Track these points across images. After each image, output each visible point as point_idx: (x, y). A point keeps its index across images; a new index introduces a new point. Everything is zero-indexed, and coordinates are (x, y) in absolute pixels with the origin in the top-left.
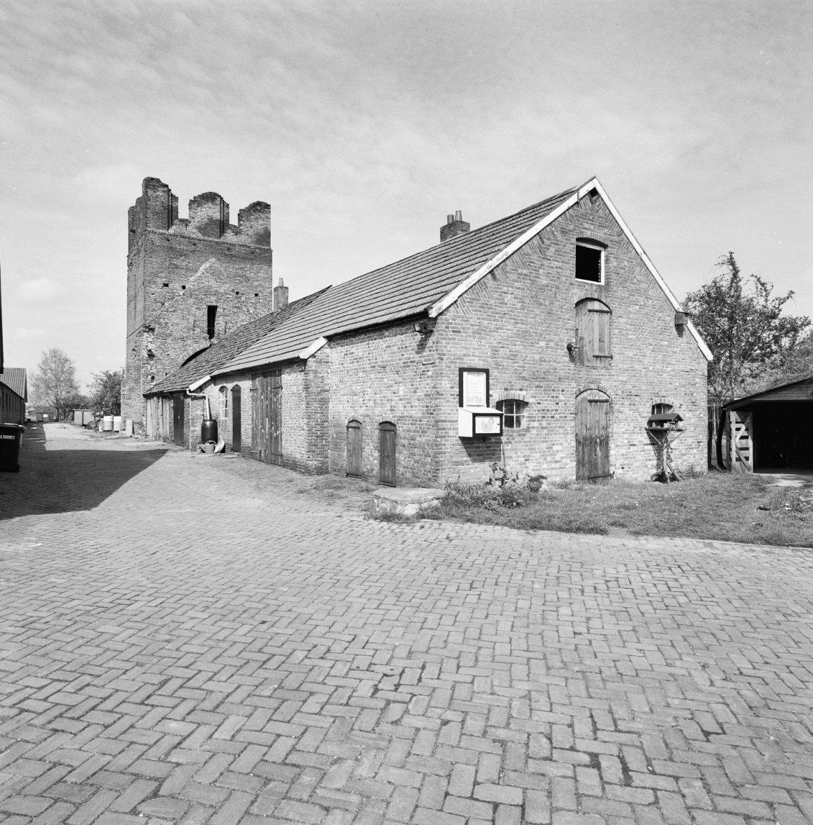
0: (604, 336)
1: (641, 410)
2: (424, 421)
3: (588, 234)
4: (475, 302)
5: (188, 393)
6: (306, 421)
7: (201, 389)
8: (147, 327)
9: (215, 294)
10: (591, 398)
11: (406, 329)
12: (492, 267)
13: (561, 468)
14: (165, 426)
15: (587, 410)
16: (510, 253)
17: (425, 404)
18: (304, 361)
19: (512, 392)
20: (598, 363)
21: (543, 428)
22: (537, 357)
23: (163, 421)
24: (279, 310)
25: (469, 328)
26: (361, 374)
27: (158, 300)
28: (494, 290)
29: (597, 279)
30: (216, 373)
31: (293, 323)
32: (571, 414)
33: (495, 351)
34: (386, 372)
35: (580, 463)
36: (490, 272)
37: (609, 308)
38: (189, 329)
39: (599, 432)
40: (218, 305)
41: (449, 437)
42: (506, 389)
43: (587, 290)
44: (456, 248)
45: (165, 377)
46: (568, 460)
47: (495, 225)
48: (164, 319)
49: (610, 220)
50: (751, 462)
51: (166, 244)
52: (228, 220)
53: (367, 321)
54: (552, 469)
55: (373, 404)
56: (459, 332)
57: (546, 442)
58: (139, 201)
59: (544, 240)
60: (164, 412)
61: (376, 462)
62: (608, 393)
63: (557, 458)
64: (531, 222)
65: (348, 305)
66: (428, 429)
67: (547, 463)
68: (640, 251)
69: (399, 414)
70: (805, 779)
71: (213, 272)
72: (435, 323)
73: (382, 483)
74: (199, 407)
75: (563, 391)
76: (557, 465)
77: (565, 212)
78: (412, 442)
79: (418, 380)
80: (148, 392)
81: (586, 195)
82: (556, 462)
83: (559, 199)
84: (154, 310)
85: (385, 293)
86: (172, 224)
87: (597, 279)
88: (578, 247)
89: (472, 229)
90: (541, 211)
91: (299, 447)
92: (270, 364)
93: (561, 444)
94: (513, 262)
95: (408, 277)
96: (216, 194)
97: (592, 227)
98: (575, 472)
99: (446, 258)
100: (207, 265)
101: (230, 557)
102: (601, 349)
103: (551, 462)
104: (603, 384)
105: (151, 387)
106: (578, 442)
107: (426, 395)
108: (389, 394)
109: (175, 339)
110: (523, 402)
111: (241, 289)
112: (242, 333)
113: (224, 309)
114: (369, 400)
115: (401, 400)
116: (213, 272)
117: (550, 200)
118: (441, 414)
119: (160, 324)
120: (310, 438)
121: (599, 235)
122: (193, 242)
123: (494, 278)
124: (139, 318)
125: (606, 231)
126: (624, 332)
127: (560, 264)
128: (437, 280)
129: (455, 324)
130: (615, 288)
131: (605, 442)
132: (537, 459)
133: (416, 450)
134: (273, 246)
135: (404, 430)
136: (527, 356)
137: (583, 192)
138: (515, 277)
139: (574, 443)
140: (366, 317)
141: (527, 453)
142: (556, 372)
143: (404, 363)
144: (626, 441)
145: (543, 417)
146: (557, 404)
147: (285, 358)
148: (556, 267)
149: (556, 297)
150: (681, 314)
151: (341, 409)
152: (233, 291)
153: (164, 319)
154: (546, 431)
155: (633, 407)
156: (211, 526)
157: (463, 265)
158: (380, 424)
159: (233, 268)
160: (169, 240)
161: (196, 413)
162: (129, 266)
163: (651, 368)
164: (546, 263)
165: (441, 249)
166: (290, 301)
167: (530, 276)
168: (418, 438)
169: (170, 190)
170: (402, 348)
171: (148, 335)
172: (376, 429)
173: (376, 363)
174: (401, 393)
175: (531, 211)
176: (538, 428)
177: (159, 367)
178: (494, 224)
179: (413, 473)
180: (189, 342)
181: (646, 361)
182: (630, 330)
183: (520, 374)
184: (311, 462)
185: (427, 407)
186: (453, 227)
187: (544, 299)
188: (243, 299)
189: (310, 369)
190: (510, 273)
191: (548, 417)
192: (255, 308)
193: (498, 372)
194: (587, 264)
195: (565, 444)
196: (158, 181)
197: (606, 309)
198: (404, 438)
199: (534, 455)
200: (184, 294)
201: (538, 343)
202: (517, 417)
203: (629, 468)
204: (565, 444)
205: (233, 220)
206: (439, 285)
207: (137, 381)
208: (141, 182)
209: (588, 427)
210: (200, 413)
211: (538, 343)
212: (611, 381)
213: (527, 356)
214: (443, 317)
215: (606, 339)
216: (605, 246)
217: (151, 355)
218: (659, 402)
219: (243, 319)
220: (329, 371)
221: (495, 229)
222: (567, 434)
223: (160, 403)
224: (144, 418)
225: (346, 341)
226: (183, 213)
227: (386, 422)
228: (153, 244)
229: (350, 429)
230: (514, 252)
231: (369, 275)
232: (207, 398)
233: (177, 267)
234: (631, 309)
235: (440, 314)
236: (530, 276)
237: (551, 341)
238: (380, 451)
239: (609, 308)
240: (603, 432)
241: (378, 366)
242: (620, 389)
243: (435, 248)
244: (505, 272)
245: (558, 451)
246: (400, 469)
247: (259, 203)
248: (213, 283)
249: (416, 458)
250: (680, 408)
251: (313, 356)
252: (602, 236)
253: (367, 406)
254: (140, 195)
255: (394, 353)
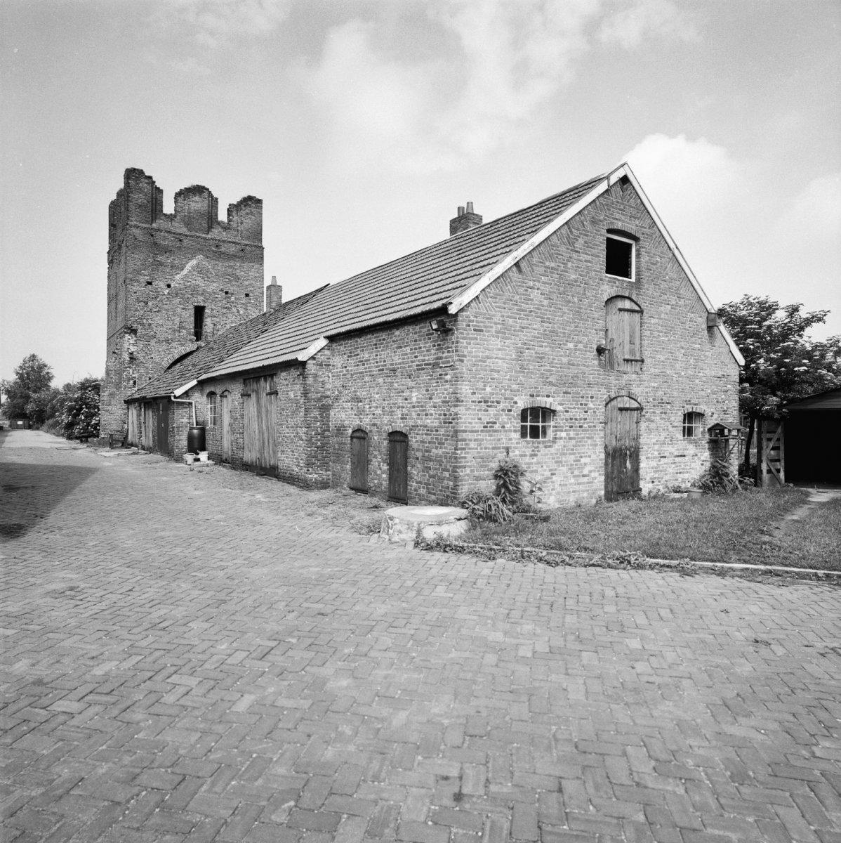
0: (634, 338)
1: (672, 419)
2: (442, 431)
3: (619, 225)
4: (498, 297)
5: (172, 398)
6: (305, 430)
7: (186, 394)
8: (129, 328)
9: (203, 294)
10: (621, 406)
11: (420, 328)
12: (517, 259)
13: (588, 483)
14: (147, 434)
15: (617, 419)
16: (536, 244)
17: (442, 412)
18: (303, 364)
19: (538, 398)
20: (628, 368)
21: (570, 438)
22: (565, 360)
23: (145, 429)
24: (272, 311)
25: (492, 327)
26: (367, 379)
27: (141, 299)
28: (519, 284)
29: (627, 274)
30: (204, 377)
31: (288, 325)
32: (601, 423)
33: (520, 352)
34: (397, 376)
35: (609, 478)
36: (515, 264)
37: (639, 306)
38: (174, 331)
39: (629, 443)
40: (206, 305)
41: (470, 449)
42: (532, 396)
43: (617, 287)
44: (470, 240)
45: (148, 382)
46: (596, 474)
47: (517, 215)
48: (147, 320)
49: (642, 210)
50: (782, 475)
51: (150, 239)
52: (217, 215)
53: (359, 324)
54: (579, 484)
55: (381, 412)
56: (482, 331)
57: (574, 454)
58: (120, 194)
59: (573, 230)
60: (147, 420)
61: (384, 476)
62: (639, 400)
63: (586, 472)
64: (558, 211)
65: (350, 303)
66: (446, 440)
67: (574, 477)
68: (672, 245)
69: (411, 423)
70: (776, 776)
71: (199, 270)
72: (456, 321)
73: (390, 499)
74: (184, 414)
75: (592, 397)
76: (585, 480)
77: (594, 201)
78: (427, 454)
79: (434, 385)
80: (130, 398)
81: (617, 182)
82: (584, 476)
83: (586, 187)
84: (137, 310)
85: (392, 290)
86: (156, 218)
87: (627, 275)
88: (608, 240)
89: (484, 222)
90: (567, 199)
91: (297, 459)
92: (269, 366)
93: (590, 456)
94: (540, 254)
95: (417, 272)
96: (204, 187)
97: (623, 218)
98: (603, 487)
99: (461, 252)
100: (194, 262)
101: (222, 596)
102: (632, 352)
103: (579, 476)
104: (636, 390)
105: (133, 392)
106: (607, 454)
107: (443, 402)
108: (400, 401)
109: (159, 342)
110: (550, 409)
111: (231, 289)
112: (231, 335)
113: (212, 310)
114: (377, 407)
115: (414, 407)
116: (199, 270)
117: (576, 188)
118: (462, 423)
119: (143, 325)
120: (309, 449)
121: (630, 227)
122: (180, 238)
123: (520, 271)
124: (120, 319)
125: (637, 222)
126: (656, 334)
127: (589, 258)
128: (454, 274)
129: (477, 322)
130: (646, 286)
131: (635, 455)
132: (564, 473)
133: (431, 463)
134: (264, 244)
135: (417, 441)
136: (554, 359)
137: (614, 179)
138: (541, 270)
139: (603, 456)
140: (373, 315)
141: (554, 466)
142: (585, 377)
143: (417, 366)
144: (656, 453)
145: (571, 427)
146: (586, 412)
147: (281, 360)
148: (586, 261)
149: (585, 294)
150: (713, 316)
151: (345, 416)
152: (222, 290)
153: (147, 320)
154: (573, 442)
155: (663, 415)
156: (198, 554)
157: (482, 258)
158: (390, 434)
159: (221, 266)
160: (152, 236)
161: (183, 421)
162: (109, 263)
163: (683, 374)
164: (575, 255)
165: (453, 242)
166: (284, 300)
167: (557, 270)
168: (434, 450)
169: (155, 182)
170: (416, 349)
171: (129, 337)
172: (384, 439)
173: (385, 365)
174: (414, 399)
175: (555, 200)
176: (565, 438)
177: (142, 371)
178: (511, 215)
179: (428, 489)
180: (174, 344)
181: (678, 366)
182: (662, 332)
183: (547, 378)
184: (310, 476)
185: (445, 415)
186: (463, 220)
187: (573, 296)
188: (233, 299)
189: (310, 372)
190: (538, 266)
191: (576, 427)
192: (246, 309)
193: (523, 376)
194: (618, 260)
195: (593, 457)
196: (141, 172)
197: (637, 308)
198: (418, 450)
199: (561, 468)
200: (169, 293)
201: (566, 345)
202: (543, 427)
203: (659, 482)
204: (593, 457)
205: (222, 216)
206: (456, 279)
207: (118, 386)
208: (123, 173)
209: (618, 438)
210: (185, 420)
211: (566, 345)
212: (643, 388)
213: (554, 359)
214: (464, 313)
215: (637, 341)
216: (636, 239)
217: (132, 358)
218: (691, 410)
219: (232, 321)
220: (330, 375)
221: (514, 220)
222: (596, 445)
223: (143, 410)
224: (126, 426)
225: (349, 342)
226: (169, 207)
227: (396, 432)
228: (136, 239)
229: (355, 440)
230: (541, 243)
231: (371, 272)
232: (193, 405)
233: (161, 264)
234: (662, 309)
235: (461, 310)
236: (557, 270)
237: (580, 342)
238: (388, 465)
239: (639, 306)
240: (633, 443)
241: (387, 369)
242: (651, 396)
243: (446, 242)
244: (531, 265)
245: (586, 464)
246: (413, 485)
247: (250, 198)
248: (200, 282)
249: (432, 472)
250: (712, 416)
251: (313, 358)
252: (633, 227)
253: (374, 414)
254: (122, 186)
255: (406, 354)
